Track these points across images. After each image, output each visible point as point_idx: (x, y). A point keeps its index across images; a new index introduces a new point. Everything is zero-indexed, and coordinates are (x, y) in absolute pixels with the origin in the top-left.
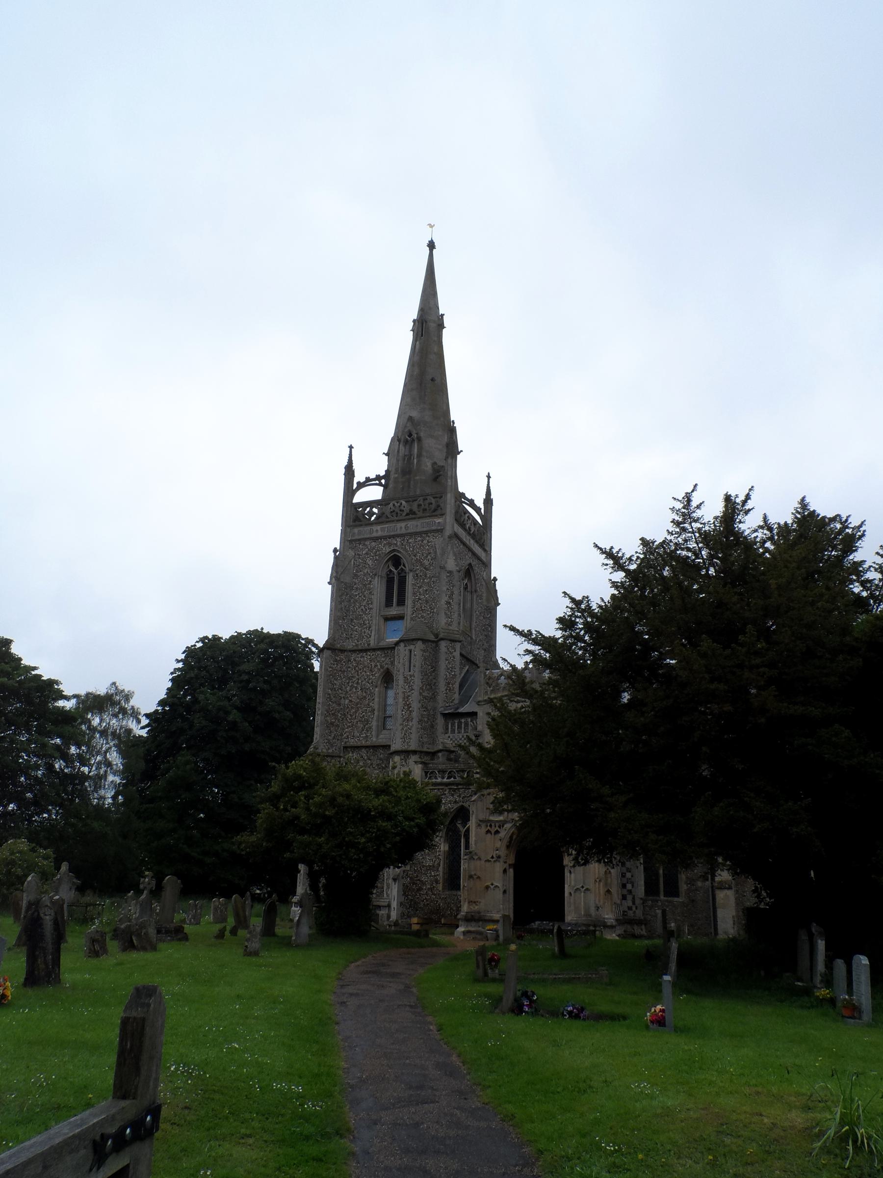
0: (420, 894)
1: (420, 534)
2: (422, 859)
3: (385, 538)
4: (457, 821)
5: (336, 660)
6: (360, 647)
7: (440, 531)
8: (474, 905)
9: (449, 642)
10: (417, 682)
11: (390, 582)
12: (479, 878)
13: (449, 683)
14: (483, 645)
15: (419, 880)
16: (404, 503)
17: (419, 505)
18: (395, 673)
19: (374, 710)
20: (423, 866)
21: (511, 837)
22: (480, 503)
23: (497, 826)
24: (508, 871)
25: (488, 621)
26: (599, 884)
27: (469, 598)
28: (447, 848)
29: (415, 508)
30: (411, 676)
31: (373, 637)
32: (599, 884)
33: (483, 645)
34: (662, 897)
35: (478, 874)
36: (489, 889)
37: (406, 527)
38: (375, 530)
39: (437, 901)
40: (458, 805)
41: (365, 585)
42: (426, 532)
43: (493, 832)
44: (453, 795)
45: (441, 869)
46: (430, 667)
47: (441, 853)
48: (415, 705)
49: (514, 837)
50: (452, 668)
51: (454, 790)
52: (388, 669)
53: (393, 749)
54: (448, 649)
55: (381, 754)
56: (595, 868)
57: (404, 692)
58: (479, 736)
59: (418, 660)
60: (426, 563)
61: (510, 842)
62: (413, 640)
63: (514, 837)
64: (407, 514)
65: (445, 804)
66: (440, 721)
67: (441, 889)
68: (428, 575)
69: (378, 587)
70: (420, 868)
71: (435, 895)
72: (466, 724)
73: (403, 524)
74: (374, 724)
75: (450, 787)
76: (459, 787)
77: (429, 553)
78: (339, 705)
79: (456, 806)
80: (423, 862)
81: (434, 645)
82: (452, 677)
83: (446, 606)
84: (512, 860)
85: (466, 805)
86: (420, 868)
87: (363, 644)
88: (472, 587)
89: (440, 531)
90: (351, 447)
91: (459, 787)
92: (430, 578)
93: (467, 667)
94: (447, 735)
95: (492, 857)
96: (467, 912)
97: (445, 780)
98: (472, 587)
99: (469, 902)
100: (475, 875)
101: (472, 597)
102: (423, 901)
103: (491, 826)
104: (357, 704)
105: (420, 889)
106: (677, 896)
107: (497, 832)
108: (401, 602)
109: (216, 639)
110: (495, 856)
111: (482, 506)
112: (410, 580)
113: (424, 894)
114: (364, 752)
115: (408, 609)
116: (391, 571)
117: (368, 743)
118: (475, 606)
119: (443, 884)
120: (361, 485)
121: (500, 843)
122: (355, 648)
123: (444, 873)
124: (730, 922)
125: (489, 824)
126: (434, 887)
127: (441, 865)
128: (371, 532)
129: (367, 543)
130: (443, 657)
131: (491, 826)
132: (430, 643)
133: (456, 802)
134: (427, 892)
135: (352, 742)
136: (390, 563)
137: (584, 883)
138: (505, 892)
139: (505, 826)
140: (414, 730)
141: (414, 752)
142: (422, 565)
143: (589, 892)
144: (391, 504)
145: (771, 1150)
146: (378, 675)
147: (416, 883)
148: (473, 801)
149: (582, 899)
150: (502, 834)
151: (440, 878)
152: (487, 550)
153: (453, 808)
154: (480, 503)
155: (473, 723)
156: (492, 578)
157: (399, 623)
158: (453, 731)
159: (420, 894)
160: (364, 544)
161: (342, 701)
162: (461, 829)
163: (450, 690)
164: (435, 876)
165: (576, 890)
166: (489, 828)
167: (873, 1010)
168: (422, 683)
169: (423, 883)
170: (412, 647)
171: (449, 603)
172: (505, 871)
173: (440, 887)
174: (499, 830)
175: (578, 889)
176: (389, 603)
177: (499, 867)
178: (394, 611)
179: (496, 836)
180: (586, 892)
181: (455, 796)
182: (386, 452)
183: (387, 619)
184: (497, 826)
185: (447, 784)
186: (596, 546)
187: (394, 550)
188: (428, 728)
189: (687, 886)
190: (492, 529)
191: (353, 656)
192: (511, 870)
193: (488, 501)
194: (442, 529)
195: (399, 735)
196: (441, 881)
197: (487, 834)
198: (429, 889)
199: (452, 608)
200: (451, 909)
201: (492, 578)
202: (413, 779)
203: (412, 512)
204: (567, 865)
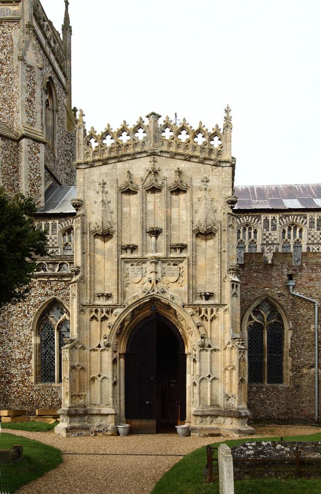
0: (10, 387)
2: (10, 352)
4: (49, 314)
7: (16, 20)
8: (78, 399)
9: (32, 141)
12: (83, 368)
13: (33, 185)
14: (65, 169)
15: (8, 373)
20: (12, 359)
21: (122, 324)
23: (104, 312)
24: (118, 360)
25: (69, 147)
26: (231, 372)
27: (51, 116)
28: (38, 341)
32: (231, 372)
33: (65, 169)
34: (266, 383)
35: (82, 364)
36: (96, 381)
39: (30, 393)
40: (50, 298)
43: (99, 319)
44: (43, 288)
45: (32, 361)
46: (11, 167)
47: (33, 346)
49: (126, 324)
50: (36, 169)
51: (45, 283)
54: (31, 149)
56: (224, 356)
58: (79, 206)
61: (121, 329)
63: (126, 324)
65: (34, 297)
67: (33, 381)
68: (5, 71)
70: (9, 361)
71: (26, 387)
72: (54, 226)
75: (40, 279)
76: (51, 279)
77: (5, 46)
79: (47, 299)
80: (11, 356)
81: (15, 144)
82: (36, 179)
83: (27, 103)
84: (122, 349)
85: (59, 298)
86: (9, 361)
88: (53, 104)
89: (16, 20)
91: (51, 279)
93: (51, 182)
95: (99, 346)
96: (69, 408)
98: (53, 104)
99: (72, 396)
100: (78, 366)
101: (53, 116)
102: (14, 393)
103: (96, 311)
105: (9, 382)
106: (268, 383)
107: (104, 318)
110: (102, 344)
113: (14, 387)
118: (57, 127)
119: (36, 376)
121: (109, 330)
123: (36, 366)
125: (94, 309)
126: (25, 379)
127: (33, 357)
130: (23, 155)
131: (96, 311)
132: (10, 141)
133: (47, 295)
134: (18, 385)
137: (211, 371)
138: (115, 384)
139: (115, 311)
143: (217, 381)
147: (5, 376)
148: (74, 282)
150: (112, 319)
151: (33, 371)
153: (44, 301)
155: (62, 225)
156: (72, 108)
159: (10, 387)
162: (54, 322)
163: (35, 192)
164: (26, 368)
165: (201, 379)
166: (94, 313)
168: (3, 182)
169: (14, 376)
171: (31, 101)
172: (114, 361)
173: (32, 379)
174: (107, 316)
175: (204, 378)
177: (107, 356)
179: (104, 322)
180: (214, 381)
181: (47, 289)
184: (104, 312)
186: (227, 111)
189: (293, 373)
190: (72, 58)
192: (122, 360)
193: (67, 27)
194: (19, 19)
196: (33, 373)
197: (91, 321)
198: (19, 381)
199: (34, 108)
200: (46, 400)
201: (72, 108)
204: (190, 354)
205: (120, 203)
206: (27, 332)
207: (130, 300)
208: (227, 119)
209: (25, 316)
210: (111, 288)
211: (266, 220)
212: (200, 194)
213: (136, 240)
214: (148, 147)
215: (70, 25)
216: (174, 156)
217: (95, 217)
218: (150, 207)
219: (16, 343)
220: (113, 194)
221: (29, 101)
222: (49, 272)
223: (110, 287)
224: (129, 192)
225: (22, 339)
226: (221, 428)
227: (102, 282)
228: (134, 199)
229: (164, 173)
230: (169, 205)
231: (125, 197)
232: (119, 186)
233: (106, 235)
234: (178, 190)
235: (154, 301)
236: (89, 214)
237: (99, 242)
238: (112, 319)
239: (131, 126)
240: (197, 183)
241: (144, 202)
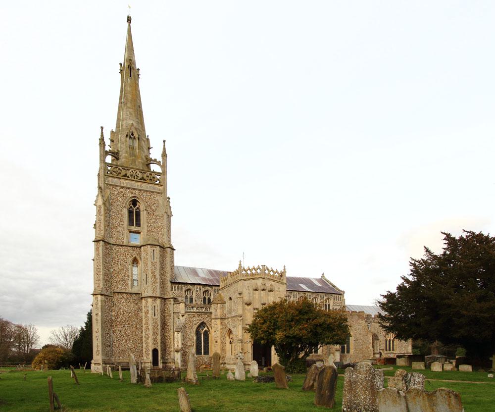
3: (129, 188)
5: (106, 248)
6: (118, 244)
11: (130, 213)
16: (138, 172)
19: (129, 276)
22: (159, 159)
29: (128, 175)
30: (155, 262)
31: (125, 239)
37: (118, 182)
38: (122, 182)
40: (202, 321)
41: (118, 211)
48: (158, 276)
52: (135, 257)
55: (135, 297)
57: (152, 270)
60: (153, 208)
62: (155, 245)
64: (140, 179)
66: (169, 284)
69: (125, 212)
72: (182, 288)
73: (139, 184)
78: (109, 271)
85: (205, 321)
87: (119, 242)
92: (157, 216)
94: (172, 292)
97: (195, 311)
104: (118, 272)
108: (138, 225)
109: (390, 297)
111: (161, 160)
114: (125, 295)
116: (131, 207)
117: (126, 291)
122: (115, 243)
128: (127, 183)
129: (118, 188)
135: (117, 290)
136: (131, 203)
140: (158, 287)
141: (159, 298)
144: (131, 171)
146: (130, 259)
149: (465, 382)
157: (138, 235)
158: (175, 290)
160: (115, 188)
161: (110, 269)
170: (154, 248)
178: (134, 228)
182: (457, 235)
183: (130, 232)
185: (196, 313)
186: (285, 267)
187: (135, 197)
191: (114, 247)
202: (492, 360)
203: (125, 175)
205: (253, 293)
206: (192, 335)
208: (285, 269)
209: (191, 328)
211: (215, 289)
212: (277, 293)
216: (270, 280)
218: (262, 295)
219: (188, 339)
220: (251, 291)
221: (168, 231)
222: (200, 311)
224: (256, 290)
225: (191, 337)
226: (134, 361)
229: (267, 285)
230: (268, 295)
233: (249, 304)
234: (270, 291)
236: (244, 297)
237: (246, 306)
240: (276, 289)
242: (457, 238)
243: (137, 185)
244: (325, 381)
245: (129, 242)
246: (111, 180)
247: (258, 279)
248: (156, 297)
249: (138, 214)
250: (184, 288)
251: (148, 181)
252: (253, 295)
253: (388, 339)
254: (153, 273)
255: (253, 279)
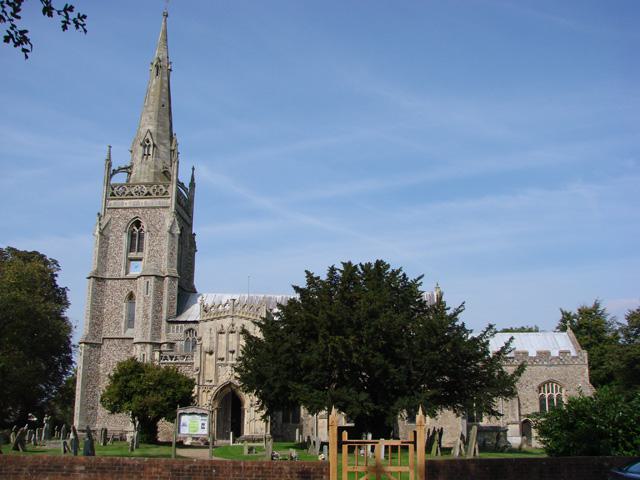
1: (154, 208)
3: (131, 208)
10: (151, 302)
11: (132, 236)
17: (154, 190)
18: (137, 295)
22: (187, 185)
29: (151, 192)
42: (158, 208)
53: (135, 341)
55: (127, 342)
59: (151, 288)
66: (164, 324)
69: (125, 238)
73: (143, 201)
74: (123, 324)
87: (115, 275)
90: (110, 147)
108: (140, 249)
112: (147, 237)
115: (145, 254)
120: (115, 172)
124: (247, 405)
141: (150, 343)
142: (155, 227)
145: (316, 392)
152: (191, 218)
154: (187, 185)
167: (13, 249)
176: (131, 248)
178: (133, 255)
188: (156, 328)
191: (109, 282)
193: (192, 184)
195: (140, 333)
203: (149, 194)
205: (217, 338)
207: (220, 383)
210: (212, 378)
213: (224, 356)
214: (230, 314)
215: (193, 232)
217: (206, 344)
218: (230, 340)
220: (214, 335)
223: (212, 378)
227: (209, 374)
228: (224, 336)
231: (171, 326)
232: (515, 400)
233: (211, 353)
235: (231, 383)
237: (207, 355)
238: (212, 392)
239: (223, 303)
241: (228, 338)
242: (193, 232)
243: (142, 202)
244: (436, 442)
245: (127, 273)
246: (112, 203)
247: (225, 317)
248: (145, 343)
249: (141, 237)
250: (185, 327)
251: (135, 196)
252: (217, 341)
253: (547, 395)
254: (145, 311)
255: (218, 319)
